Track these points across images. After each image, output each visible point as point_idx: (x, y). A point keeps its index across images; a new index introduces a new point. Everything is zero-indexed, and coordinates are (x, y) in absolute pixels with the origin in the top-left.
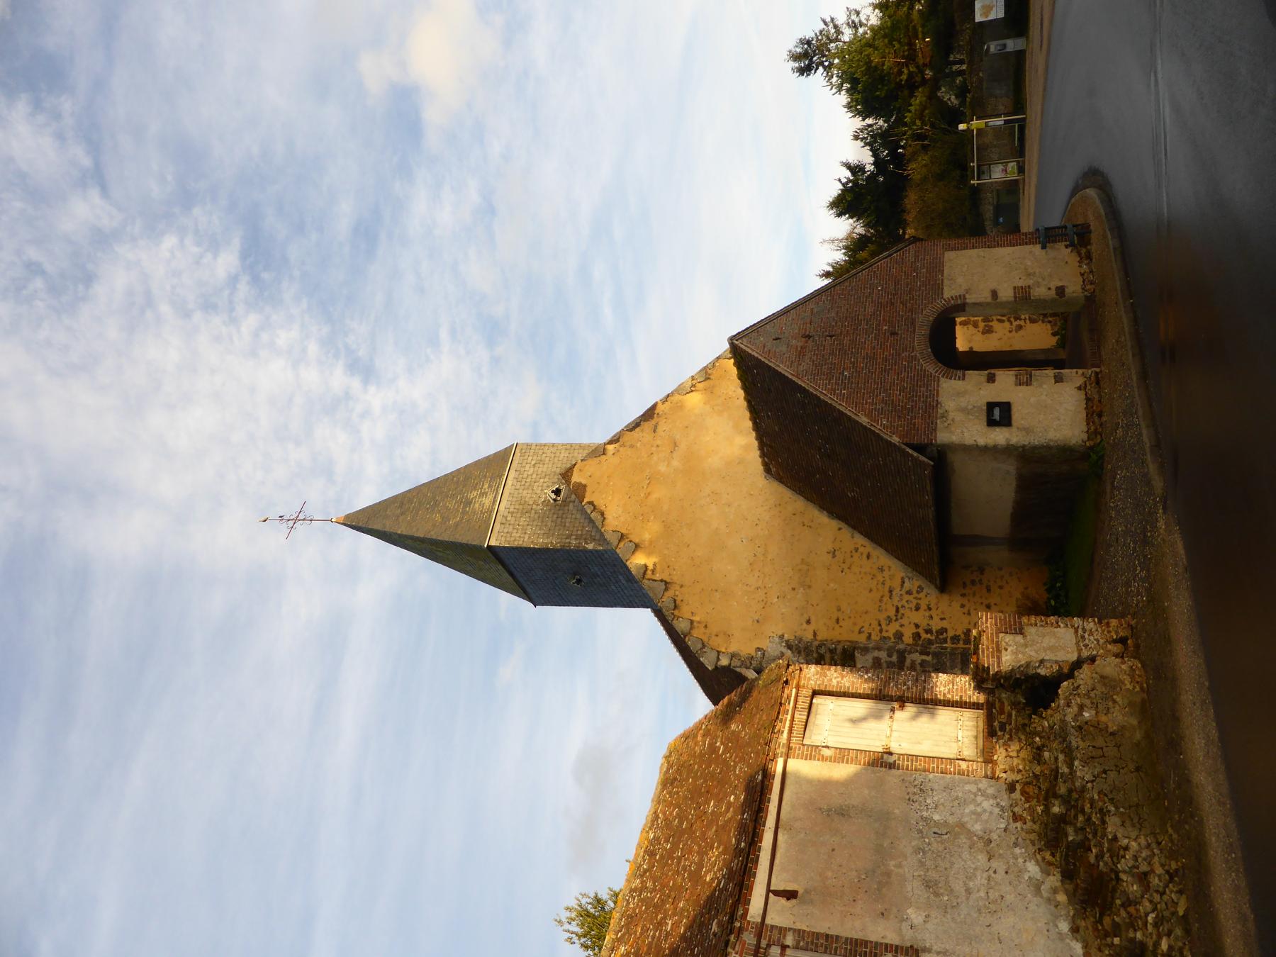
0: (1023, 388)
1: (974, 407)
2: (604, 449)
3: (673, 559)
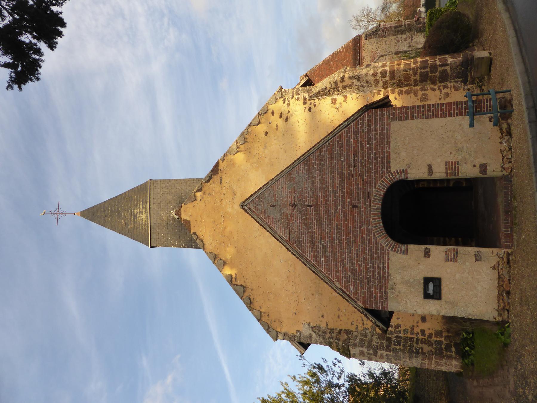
0: (449, 263)
1: (415, 280)
2: (195, 196)
3: (245, 272)
